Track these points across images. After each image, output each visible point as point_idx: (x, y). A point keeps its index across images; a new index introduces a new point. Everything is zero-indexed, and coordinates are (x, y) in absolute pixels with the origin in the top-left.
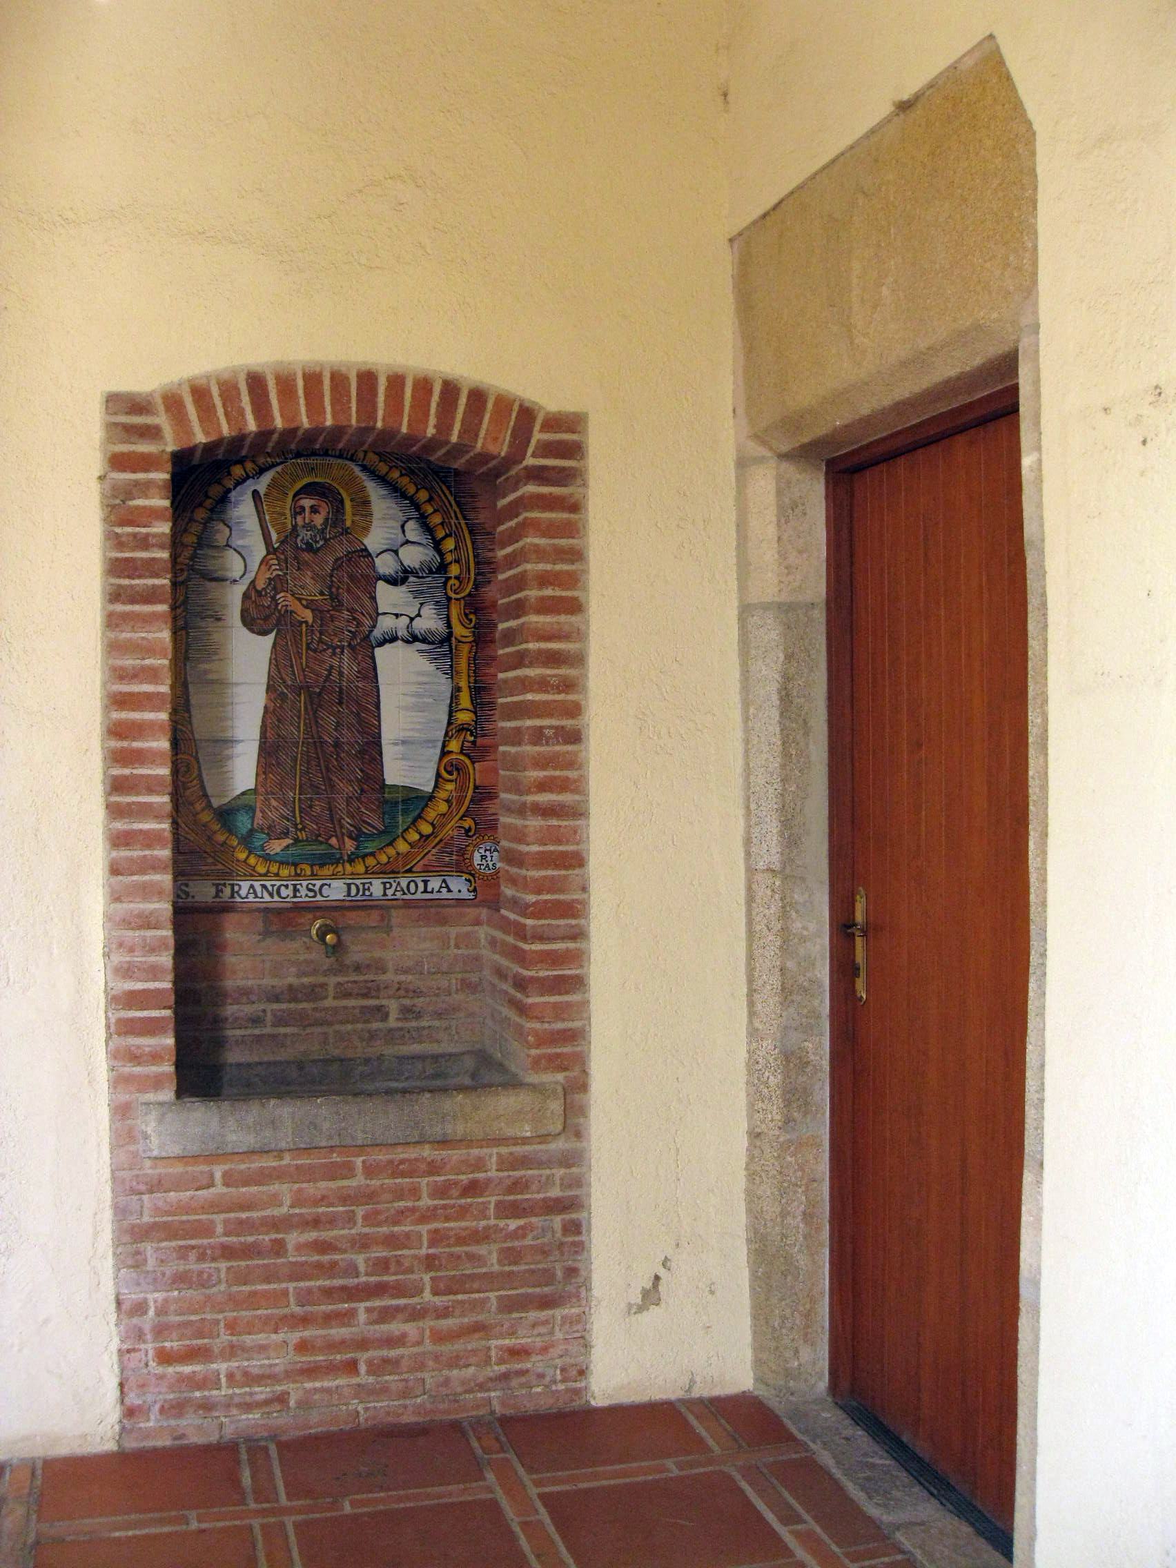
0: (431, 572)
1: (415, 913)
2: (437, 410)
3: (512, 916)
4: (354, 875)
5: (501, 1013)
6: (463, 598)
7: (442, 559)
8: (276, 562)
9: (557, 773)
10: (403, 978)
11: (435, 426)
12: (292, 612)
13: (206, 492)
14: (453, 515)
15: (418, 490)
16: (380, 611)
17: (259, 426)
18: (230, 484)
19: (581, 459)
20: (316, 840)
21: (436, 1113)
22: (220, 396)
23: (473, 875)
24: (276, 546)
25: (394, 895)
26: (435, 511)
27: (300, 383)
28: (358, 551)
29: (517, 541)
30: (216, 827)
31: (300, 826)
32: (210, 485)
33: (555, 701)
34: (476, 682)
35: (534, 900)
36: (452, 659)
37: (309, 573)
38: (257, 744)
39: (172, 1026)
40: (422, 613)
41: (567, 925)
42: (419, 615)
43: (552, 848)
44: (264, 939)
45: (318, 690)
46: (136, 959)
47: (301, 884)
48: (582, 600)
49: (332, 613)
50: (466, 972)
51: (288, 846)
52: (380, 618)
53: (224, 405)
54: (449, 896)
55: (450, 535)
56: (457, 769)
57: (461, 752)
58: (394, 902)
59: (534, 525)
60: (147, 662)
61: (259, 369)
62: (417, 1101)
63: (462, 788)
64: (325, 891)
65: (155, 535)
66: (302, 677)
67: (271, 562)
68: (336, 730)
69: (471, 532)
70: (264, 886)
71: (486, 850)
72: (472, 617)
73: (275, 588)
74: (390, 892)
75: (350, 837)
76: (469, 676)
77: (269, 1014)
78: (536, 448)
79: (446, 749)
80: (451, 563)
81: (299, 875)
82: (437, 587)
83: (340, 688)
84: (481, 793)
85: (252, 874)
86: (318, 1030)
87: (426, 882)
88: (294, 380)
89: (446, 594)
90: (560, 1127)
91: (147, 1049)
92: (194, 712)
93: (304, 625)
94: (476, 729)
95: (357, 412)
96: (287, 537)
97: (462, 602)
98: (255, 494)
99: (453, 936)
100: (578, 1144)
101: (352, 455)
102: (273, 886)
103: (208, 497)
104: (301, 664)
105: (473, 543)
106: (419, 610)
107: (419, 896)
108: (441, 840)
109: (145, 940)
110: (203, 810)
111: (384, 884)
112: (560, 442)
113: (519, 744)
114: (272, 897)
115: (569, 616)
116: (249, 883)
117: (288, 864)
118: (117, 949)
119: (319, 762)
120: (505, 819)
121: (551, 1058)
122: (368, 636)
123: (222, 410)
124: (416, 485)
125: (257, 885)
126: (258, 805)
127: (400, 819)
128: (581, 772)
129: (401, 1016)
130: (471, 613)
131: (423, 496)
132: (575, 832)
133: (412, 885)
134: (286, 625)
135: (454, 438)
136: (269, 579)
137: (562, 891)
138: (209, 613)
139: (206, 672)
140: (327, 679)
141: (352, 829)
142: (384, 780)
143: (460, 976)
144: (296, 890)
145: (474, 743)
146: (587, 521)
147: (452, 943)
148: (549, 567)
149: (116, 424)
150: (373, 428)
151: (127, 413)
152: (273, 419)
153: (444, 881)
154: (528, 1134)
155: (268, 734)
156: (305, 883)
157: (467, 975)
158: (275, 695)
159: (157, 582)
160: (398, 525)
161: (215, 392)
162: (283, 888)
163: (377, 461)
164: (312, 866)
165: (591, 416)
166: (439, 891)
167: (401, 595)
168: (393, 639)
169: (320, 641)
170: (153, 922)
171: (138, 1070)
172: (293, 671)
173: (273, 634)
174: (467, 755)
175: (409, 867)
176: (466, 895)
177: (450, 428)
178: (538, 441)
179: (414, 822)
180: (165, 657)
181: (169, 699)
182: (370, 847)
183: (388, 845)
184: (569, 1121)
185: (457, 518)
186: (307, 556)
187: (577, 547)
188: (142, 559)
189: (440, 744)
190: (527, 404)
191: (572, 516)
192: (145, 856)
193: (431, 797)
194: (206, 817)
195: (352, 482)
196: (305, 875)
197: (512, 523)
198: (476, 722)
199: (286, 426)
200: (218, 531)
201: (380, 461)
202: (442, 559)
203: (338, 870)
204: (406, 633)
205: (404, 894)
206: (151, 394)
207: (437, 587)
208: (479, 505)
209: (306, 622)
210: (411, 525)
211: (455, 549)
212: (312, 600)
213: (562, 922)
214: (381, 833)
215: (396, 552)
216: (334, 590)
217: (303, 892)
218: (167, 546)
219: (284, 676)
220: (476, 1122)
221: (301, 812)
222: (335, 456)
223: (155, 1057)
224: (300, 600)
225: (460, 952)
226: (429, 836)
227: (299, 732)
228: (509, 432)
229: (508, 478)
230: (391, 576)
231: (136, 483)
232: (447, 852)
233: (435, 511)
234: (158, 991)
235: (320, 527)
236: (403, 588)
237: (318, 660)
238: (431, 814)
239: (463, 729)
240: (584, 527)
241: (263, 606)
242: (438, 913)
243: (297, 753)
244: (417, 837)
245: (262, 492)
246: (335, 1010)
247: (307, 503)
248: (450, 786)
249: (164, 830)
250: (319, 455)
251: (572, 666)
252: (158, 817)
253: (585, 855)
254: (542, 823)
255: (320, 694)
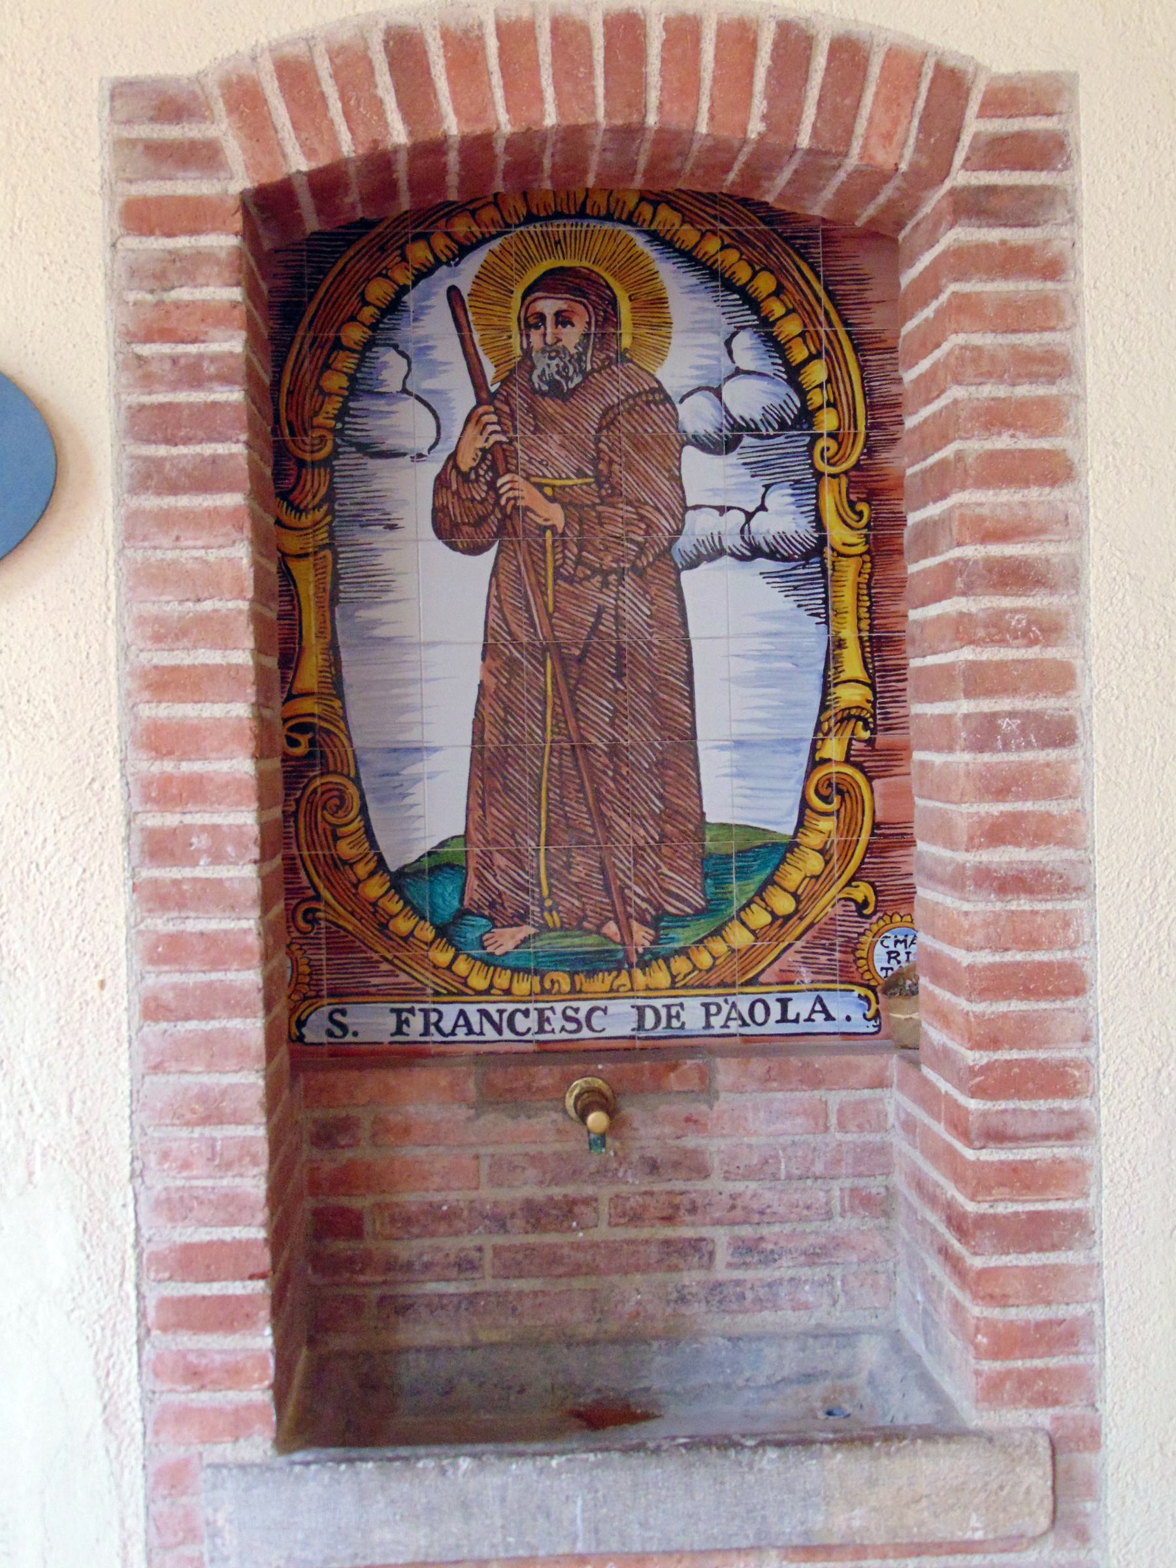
0: (783, 426)
1: (758, 1066)
2: (768, 82)
3: (944, 1086)
4: (652, 990)
5: (925, 1267)
6: (846, 473)
7: (804, 401)
8: (494, 418)
9: (1028, 806)
10: (739, 1186)
11: (764, 118)
12: (527, 509)
13: (362, 294)
14: (822, 318)
15: (755, 274)
16: (690, 503)
17: (411, 133)
18: (403, 277)
19: (1065, 168)
20: (580, 928)
21: (791, 1491)
22: (335, 76)
23: (873, 989)
24: (493, 389)
25: (725, 1026)
26: (789, 312)
27: (492, 44)
28: (646, 392)
29: (938, 346)
30: (395, 906)
31: (548, 903)
32: (368, 280)
33: (1024, 662)
34: (872, 628)
35: (984, 1061)
36: (826, 587)
37: (556, 437)
38: (467, 753)
39: (265, 1314)
40: (767, 504)
41: (1051, 1111)
42: (762, 508)
43: (1019, 957)
44: (478, 1116)
45: (577, 652)
46: (195, 1183)
47: (552, 1009)
48: (1074, 455)
49: (599, 508)
50: (860, 1175)
51: (525, 941)
52: (690, 515)
53: (343, 98)
54: (829, 1027)
55: (818, 356)
56: (840, 792)
57: (847, 761)
58: (726, 1040)
59: (965, 307)
60: (207, 606)
61: (409, 20)
62: (751, 1466)
63: (850, 827)
64: (597, 1020)
65: (214, 358)
66: (546, 629)
67: (485, 419)
68: (612, 724)
69: (856, 348)
70: (484, 1013)
71: (896, 942)
72: (863, 507)
73: (493, 467)
74: (717, 1021)
75: (643, 922)
76: (859, 619)
77: (488, 1255)
78: (973, 148)
79: (818, 757)
80: (821, 407)
81: (549, 992)
82: (795, 455)
83: (619, 647)
84: (885, 836)
85: (460, 990)
86: (578, 1283)
87: (784, 1003)
88: (481, 38)
89: (812, 466)
90: (1044, 1521)
91: (218, 1358)
92: (351, 696)
93: (549, 533)
94: (874, 716)
95: (606, 97)
96: (512, 371)
97: (844, 481)
98: (453, 294)
99: (833, 1108)
100: (1082, 1554)
101: (631, 214)
102: (501, 1012)
103: (366, 303)
104: (546, 605)
105: (862, 368)
106: (763, 497)
107: (772, 1027)
108: (811, 926)
109: (213, 1147)
110: (372, 874)
111: (706, 1006)
112: (1020, 136)
113: (951, 749)
114: (500, 1032)
115: (1047, 490)
116: (456, 1008)
117: (527, 971)
118: (160, 1163)
119: (582, 785)
120: (926, 893)
121: (1024, 1380)
122: (668, 550)
123: (339, 105)
124: (750, 264)
125: (472, 1011)
126: (472, 864)
127: (735, 886)
128: (1078, 804)
129: (736, 1260)
130: (860, 500)
131: (765, 284)
132: (1067, 925)
133: (759, 1009)
134: (516, 534)
135: (804, 140)
136: (483, 450)
137: (1040, 1044)
138: (376, 515)
139: (377, 623)
140: (594, 628)
141: (644, 905)
142: (703, 814)
143: (848, 1183)
144: (542, 1020)
145: (870, 742)
146: (1079, 293)
147: (833, 1120)
148: (1002, 391)
149: (132, 143)
150: (641, 128)
151: (152, 119)
152: (440, 119)
153: (819, 1000)
154: (979, 1535)
155: (487, 736)
156: (560, 1007)
157: (861, 1182)
158: (499, 663)
159: (221, 449)
160: (718, 340)
161: (324, 68)
162: (519, 1016)
163: (677, 222)
164: (572, 974)
165: (1084, 81)
166: (809, 1019)
167: (730, 471)
168: (719, 553)
169: (579, 561)
170: (228, 1111)
171: (204, 1398)
172: (531, 618)
173: (491, 554)
174: (859, 766)
175: (750, 975)
176: (860, 1025)
177: (794, 119)
178: (976, 136)
179: (761, 892)
180: (240, 596)
181: (251, 677)
182: (682, 937)
183: (712, 934)
184: (1062, 1507)
185: (830, 324)
186: (551, 406)
187: (1058, 349)
188: (190, 405)
189: (806, 747)
190: (950, 63)
191: (1050, 285)
192: (210, 984)
193: (792, 846)
194: (374, 889)
195: (630, 263)
196: (559, 992)
197: (928, 312)
198: (874, 707)
199: (467, 130)
200: (385, 365)
201: (683, 222)
202: (804, 401)
203: (618, 982)
204: (739, 542)
205: (745, 1024)
206: (197, 79)
207: (795, 455)
208: (869, 296)
209: (553, 528)
210: (744, 341)
211: (829, 381)
212: (563, 487)
213: (1042, 1105)
214: (699, 913)
215: (718, 393)
216: (601, 466)
217: (557, 1022)
218: (239, 379)
219: (514, 627)
220: (874, 1509)
221: (549, 876)
222: (599, 218)
223: (234, 1375)
224: (540, 487)
225: (849, 1137)
226: (788, 918)
227: (544, 730)
228: (916, 122)
229: (918, 224)
230: (708, 436)
231: (174, 256)
232: (823, 946)
233: (789, 312)
234: (242, 1247)
235: (573, 351)
236: (733, 458)
237: (577, 597)
238: (793, 877)
239: (849, 718)
240: (1074, 306)
241: (473, 499)
242: (805, 1066)
243: (541, 768)
244: (767, 918)
245: (465, 289)
246: (613, 1249)
247: (548, 306)
248: (827, 824)
249: (246, 932)
250: (569, 217)
251: (1053, 588)
252: (232, 906)
253: (1087, 968)
254: (999, 906)
255: (580, 660)
